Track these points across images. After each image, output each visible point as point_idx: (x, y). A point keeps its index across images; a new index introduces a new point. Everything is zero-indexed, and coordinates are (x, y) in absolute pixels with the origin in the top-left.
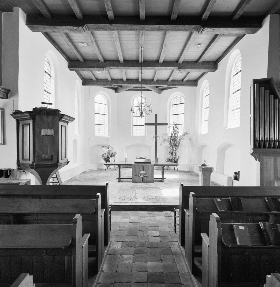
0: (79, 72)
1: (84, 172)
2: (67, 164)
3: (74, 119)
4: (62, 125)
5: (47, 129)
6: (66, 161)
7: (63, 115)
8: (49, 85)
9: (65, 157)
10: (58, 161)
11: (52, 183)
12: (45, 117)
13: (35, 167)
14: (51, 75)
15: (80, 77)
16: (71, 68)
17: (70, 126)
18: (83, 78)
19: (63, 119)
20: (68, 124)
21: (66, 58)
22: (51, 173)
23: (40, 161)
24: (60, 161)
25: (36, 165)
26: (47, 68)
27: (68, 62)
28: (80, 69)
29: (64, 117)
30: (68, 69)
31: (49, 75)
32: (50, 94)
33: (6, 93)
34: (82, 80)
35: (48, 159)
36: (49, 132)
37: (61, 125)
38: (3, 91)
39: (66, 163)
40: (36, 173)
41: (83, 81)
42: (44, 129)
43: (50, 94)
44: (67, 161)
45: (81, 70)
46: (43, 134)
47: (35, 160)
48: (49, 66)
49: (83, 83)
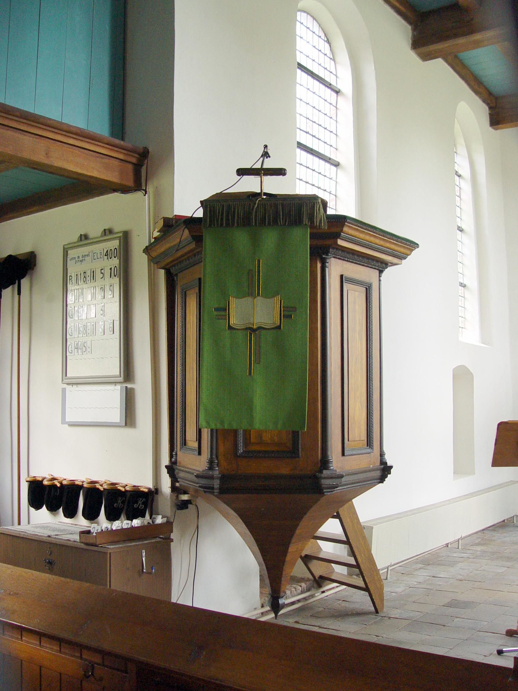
0: (461, 61)
1: (503, 525)
2: (382, 479)
3: (412, 245)
4: (346, 274)
5: (249, 299)
6: (378, 463)
7: (340, 221)
8: (334, 130)
9: (369, 443)
10: (325, 463)
11: (345, 568)
12: (241, 238)
13: (216, 484)
14: (340, 86)
15: (476, 92)
16: (425, 49)
17: (393, 281)
18: (490, 94)
19: (340, 242)
20: (381, 272)
21: (397, 5)
22: (300, 518)
23: (241, 456)
24: (337, 463)
25: (223, 478)
26: (322, 59)
27: (410, 23)
28: (461, 41)
29: (345, 229)
30: (413, 56)
31: (328, 85)
32: (337, 165)
33: (130, 167)
34: (488, 104)
35: (275, 448)
36: (262, 311)
37: (342, 276)
38: (121, 156)
39: (378, 473)
40: (236, 514)
41: (490, 108)
42: (241, 295)
43: (337, 165)
44: (383, 463)
45: (467, 49)
46: (232, 322)
47: (222, 449)
48: (328, 52)
49: (491, 115)
